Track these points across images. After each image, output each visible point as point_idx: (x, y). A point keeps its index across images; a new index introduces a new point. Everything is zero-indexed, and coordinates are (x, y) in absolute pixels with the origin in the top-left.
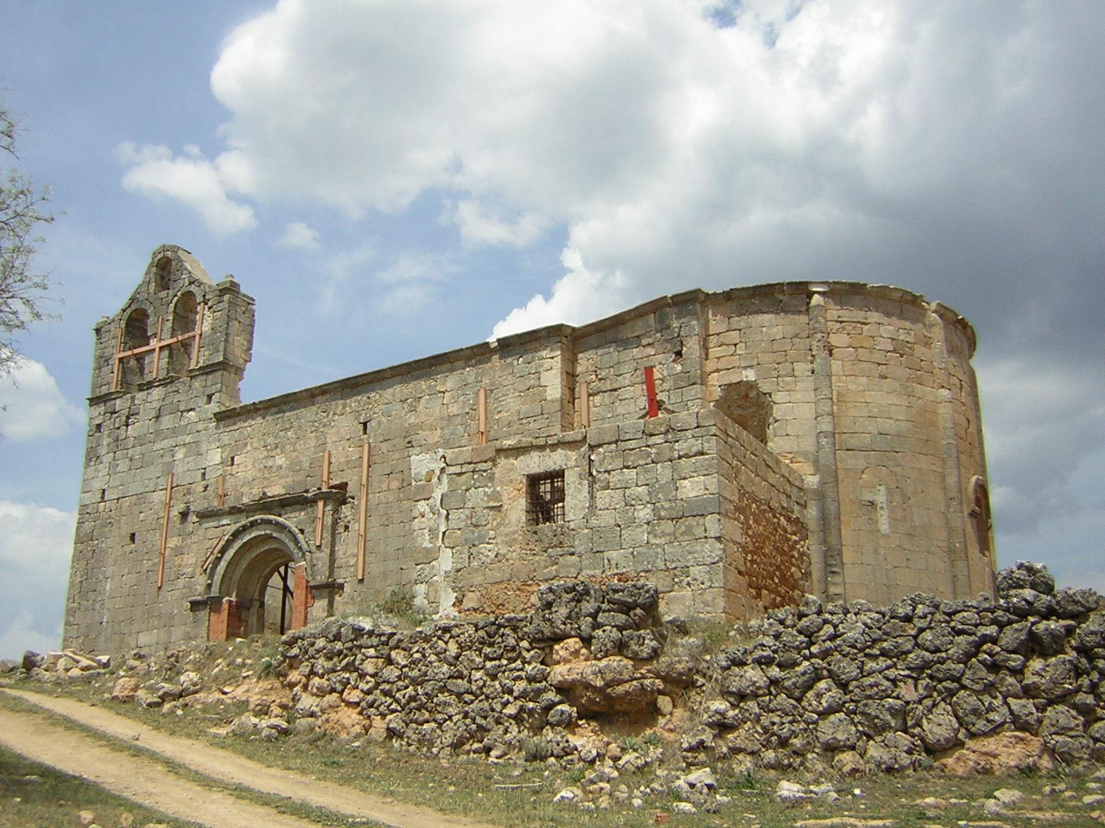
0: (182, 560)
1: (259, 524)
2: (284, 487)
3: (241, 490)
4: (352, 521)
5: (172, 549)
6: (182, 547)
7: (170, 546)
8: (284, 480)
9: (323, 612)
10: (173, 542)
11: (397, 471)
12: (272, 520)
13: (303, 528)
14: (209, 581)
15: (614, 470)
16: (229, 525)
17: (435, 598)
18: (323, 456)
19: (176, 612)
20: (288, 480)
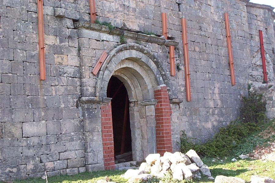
0: (62, 59)
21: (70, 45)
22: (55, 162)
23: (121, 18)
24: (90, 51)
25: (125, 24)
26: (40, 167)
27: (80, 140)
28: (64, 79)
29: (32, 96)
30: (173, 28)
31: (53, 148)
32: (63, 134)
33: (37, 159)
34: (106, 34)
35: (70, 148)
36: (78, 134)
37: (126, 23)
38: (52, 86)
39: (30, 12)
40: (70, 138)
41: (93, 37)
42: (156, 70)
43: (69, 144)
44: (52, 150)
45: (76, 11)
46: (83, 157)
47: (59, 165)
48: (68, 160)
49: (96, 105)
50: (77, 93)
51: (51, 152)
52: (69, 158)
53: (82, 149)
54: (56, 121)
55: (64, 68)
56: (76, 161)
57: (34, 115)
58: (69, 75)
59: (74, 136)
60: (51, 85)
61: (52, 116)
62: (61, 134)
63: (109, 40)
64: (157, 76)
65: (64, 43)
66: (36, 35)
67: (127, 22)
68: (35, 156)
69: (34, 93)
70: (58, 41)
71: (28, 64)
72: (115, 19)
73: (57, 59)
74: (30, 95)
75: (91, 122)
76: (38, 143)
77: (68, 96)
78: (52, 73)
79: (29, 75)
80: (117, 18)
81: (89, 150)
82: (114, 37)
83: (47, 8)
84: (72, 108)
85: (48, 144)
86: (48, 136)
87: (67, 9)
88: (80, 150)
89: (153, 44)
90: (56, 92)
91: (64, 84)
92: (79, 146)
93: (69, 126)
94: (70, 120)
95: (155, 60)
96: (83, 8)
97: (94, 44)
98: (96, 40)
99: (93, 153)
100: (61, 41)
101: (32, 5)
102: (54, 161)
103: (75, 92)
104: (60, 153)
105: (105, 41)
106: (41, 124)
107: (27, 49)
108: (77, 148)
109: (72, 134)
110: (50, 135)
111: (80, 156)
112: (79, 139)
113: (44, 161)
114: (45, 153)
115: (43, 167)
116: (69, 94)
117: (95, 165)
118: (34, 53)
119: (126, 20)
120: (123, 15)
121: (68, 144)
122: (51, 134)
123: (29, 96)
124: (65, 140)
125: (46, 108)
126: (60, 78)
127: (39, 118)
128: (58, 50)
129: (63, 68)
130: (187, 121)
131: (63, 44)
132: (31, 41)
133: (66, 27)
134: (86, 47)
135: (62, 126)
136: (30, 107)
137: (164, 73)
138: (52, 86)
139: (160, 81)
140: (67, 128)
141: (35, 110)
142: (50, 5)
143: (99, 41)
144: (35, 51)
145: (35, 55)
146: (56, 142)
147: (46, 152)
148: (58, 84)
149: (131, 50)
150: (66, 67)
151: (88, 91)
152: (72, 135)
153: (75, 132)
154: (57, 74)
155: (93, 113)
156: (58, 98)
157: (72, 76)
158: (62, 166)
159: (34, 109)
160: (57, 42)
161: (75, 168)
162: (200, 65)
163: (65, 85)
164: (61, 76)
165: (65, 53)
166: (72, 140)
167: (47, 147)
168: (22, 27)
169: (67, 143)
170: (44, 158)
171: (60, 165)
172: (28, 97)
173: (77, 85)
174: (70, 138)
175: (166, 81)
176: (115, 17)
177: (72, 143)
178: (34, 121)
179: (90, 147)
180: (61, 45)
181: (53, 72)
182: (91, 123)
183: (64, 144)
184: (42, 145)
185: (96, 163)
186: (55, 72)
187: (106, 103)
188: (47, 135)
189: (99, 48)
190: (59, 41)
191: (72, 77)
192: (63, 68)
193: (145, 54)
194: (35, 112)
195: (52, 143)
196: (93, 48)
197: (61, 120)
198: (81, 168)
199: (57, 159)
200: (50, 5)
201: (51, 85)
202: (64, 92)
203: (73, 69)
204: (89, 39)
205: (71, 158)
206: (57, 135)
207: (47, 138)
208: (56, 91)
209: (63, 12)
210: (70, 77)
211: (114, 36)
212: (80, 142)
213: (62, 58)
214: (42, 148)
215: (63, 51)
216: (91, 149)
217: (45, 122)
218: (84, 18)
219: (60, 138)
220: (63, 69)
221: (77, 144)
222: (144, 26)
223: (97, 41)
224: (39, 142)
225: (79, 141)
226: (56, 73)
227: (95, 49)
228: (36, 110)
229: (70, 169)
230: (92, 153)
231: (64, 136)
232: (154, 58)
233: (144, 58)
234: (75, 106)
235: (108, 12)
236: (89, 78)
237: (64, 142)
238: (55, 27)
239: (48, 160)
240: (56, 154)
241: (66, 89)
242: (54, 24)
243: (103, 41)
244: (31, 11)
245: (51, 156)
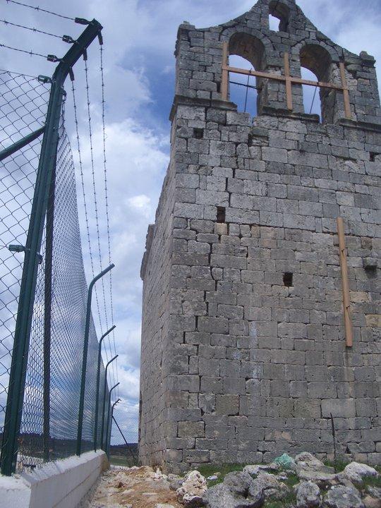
18: (341, 271)
33: (342, 447)
70: (370, 297)
100: (374, 298)
118: (336, 314)
170: (352, 446)
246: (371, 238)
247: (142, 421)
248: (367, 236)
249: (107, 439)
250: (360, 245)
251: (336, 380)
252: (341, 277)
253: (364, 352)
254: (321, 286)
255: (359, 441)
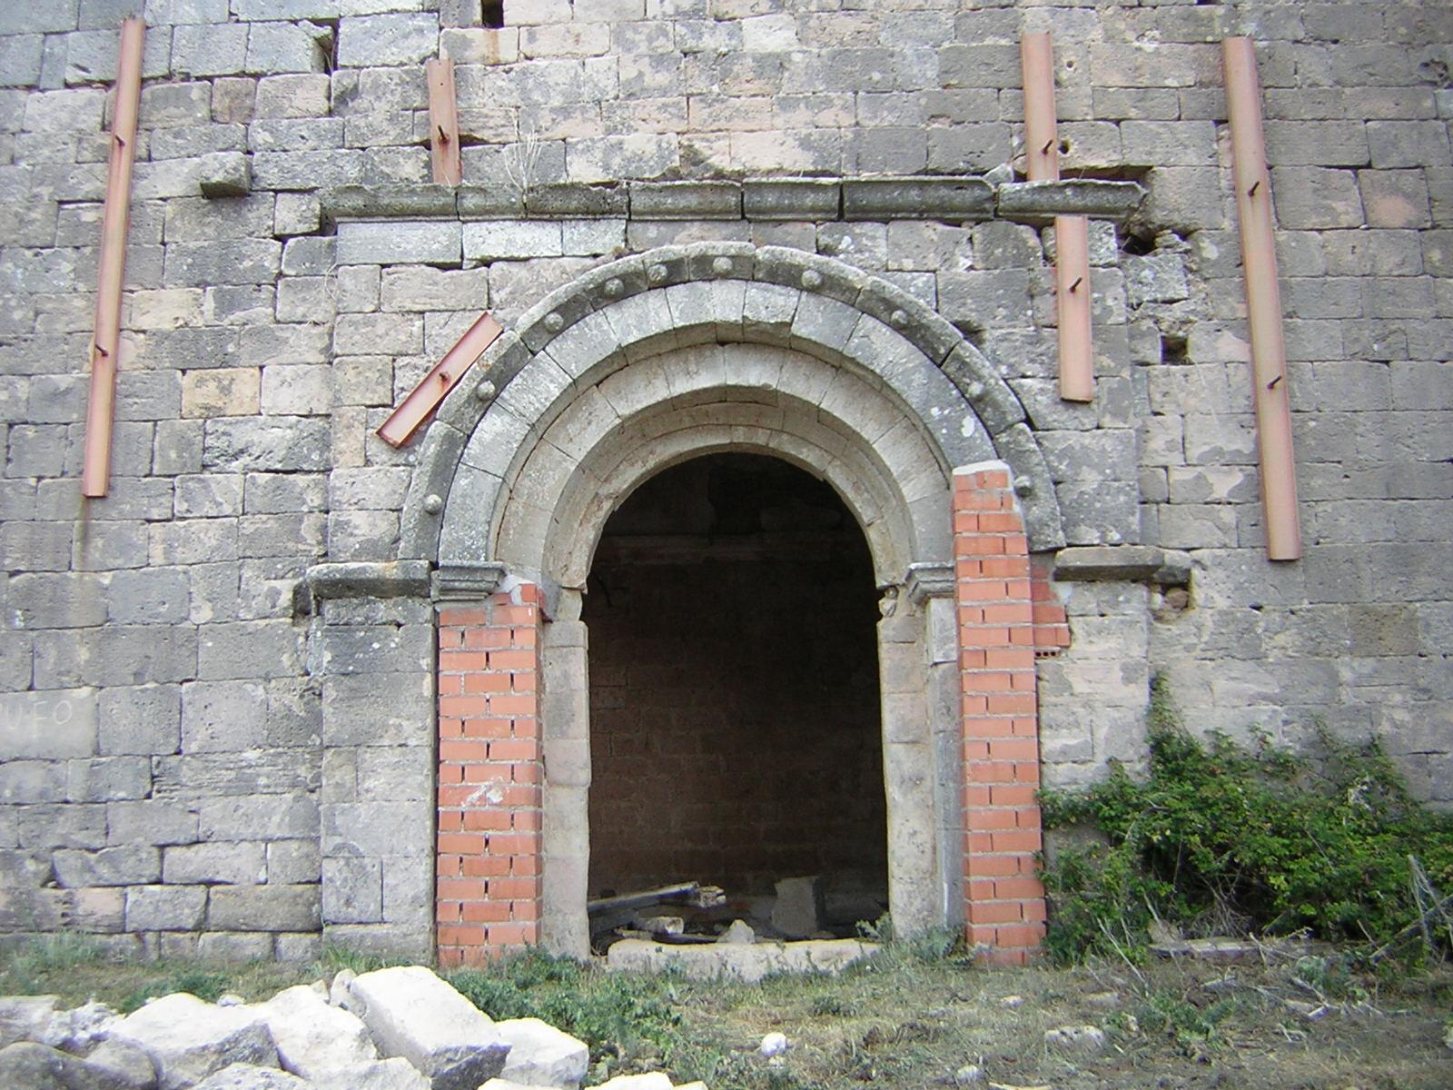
0: (225, 390)
1: (725, 276)
2: (805, 144)
3: (559, 132)
4: (1201, 324)
5: (160, 337)
6: (220, 336)
7: (146, 322)
8: (801, 115)
9: (1128, 680)
10: (167, 308)
11: (1395, 160)
12: (800, 269)
13: (973, 317)
14: (433, 499)
15: (1360, 189)
16: (564, 252)
17: (724, 154)
18: (99, 226)
19: (203, 614)
20: (826, 118)
21: (278, 317)
22: (129, 889)
23: (660, 127)
24: (381, 329)
25: (696, 153)
26: (44, 904)
27: (297, 791)
28: (227, 485)
29: (33, 572)
30: (1133, 113)
31: (122, 821)
32: (192, 755)
33: (31, 866)
34: (508, 223)
35: (225, 827)
36: (286, 759)
37: (697, 145)
38: (149, 521)
39: (73, 206)
40: (232, 774)
41: (406, 253)
42: (919, 378)
43: (225, 807)
44: (119, 831)
45: (343, 147)
46: (309, 882)
47: (150, 909)
48: (213, 889)
49: (396, 605)
50: (301, 547)
51: (111, 840)
52: (218, 878)
53: (303, 839)
54: (155, 690)
55: (233, 432)
56: (259, 898)
57: (36, 661)
58: (262, 463)
59: (263, 765)
60: (144, 516)
61: (134, 667)
62: (178, 753)
63: (524, 255)
64: (935, 411)
65: (242, 314)
66: (89, 300)
67: (712, 136)
68: (18, 852)
69: (45, 561)
70: (209, 304)
71: (30, 432)
72: (613, 138)
73: (196, 391)
74: (22, 568)
75: (355, 695)
76: (42, 794)
77: (240, 567)
78: (157, 459)
79: (33, 481)
80: (630, 129)
81: (327, 844)
82: (567, 235)
83: (168, 170)
84: (263, 623)
85: (92, 800)
86: (104, 759)
87: (285, 151)
88: (294, 845)
89: (894, 228)
90: (169, 550)
91: (225, 505)
92: (287, 819)
93: (226, 714)
94: (239, 688)
95: (897, 315)
96: (385, 123)
97: (413, 287)
98: (429, 265)
99: (347, 864)
100: (226, 304)
101: (90, 171)
102: (125, 886)
103: (290, 545)
104: (168, 849)
105: (500, 264)
106: (67, 702)
107: (36, 365)
108: (273, 831)
109: (252, 755)
110: (109, 759)
111: (289, 871)
112: (294, 786)
113: (66, 878)
114: (76, 842)
115: (60, 909)
116: (249, 553)
117: (361, 929)
118: (63, 381)
119: (698, 131)
120: (676, 104)
121: (214, 811)
122: (119, 751)
123: (22, 576)
124: (200, 787)
125: (104, 627)
126: (203, 481)
127: (60, 674)
128: (198, 351)
129: (224, 434)
130: (1266, 698)
131: (239, 316)
132: (61, 328)
133: (268, 233)
134: (357, 309)
135: (189, 712)
136: (19, 623)
137: (976, 389)
138: (149, 521)
139: (964, 439)
140: (218, 727)
141: (42, 639)
142: (183, 153)
143: (459, 267)
144: (74, 368)
145: (68, 391)
146: (142, 793)
147: (82, 838)
148: (188, 511)
149: (700, 284)
150: (242, 427)
151: (351, 535)
152: (244, 764)
153: (272, 746)
154: (185, 465)
155: (376, 646)
156: (181, 577)
157: (279, 466)
158: (167, 918)
159: (34, 634)
160: (202, 313)
161: (251, 935)
162: (1428, 311)
163: (227, 510)
164: (214, 469)
165: (244, 360)
166: (244, 786)
167: (91, 811)
168: (19, 276)
169: (211, 801)
170: (67, 863)
171: (157, 909)
172: (14, 581)
173: (305, 509)
174: (232, 774)
175: (1003, 438)
176: (609, 131)
177: (242, 801)
178: (30, 688)
179: (333, 830)
180: (226, 322)
181: (164, 457)
182: (349, 699)
183: (193, 805)
184: (67, 802)
185: (364, 919)
186: (173, 455)
187: (461, 590)
188: (97, 752)
189: (451, 304)
190: (213, 305)
191: (277, 471)
192: (229, 429)
193: (813, 290)
194: (39, 647)
195: (122, 794)
196: (408, 305)
197: (186, 685)
198: (291, 936)
199: (141, 876)
200: (183, 153)
201: (148, 516)
202: (218, 548)
203: (288, 431)
204: (383, 266)
205: (229, 880)
206: (155, 759)
207: (93, 772)
208: (171, 546)
209: (228, 165)
210: (268, 471)
211: (566, 227)
212: (296, 799)
213: (226, 383)
214: (61, 819)
215: (231, 348)
216: (338, 840)
217: (93, 694)
218: (387, 170)
219: (173, 772)
220: (225, 438)
221: (276, 812)
222: (857, 135)
223: (444, 267)
224: (50, 785)
225: (289, 796)
226: (180, 456)
227: (422, 313)
228: (49, 636)
229: (220, 934)
230: (342, 862)
231: (195, 763)
232: (891, 306)
233: (813, 320)
234: (284, 616)
235: (564, 112)
236: (361, 462)
237: (192, 794)
238: (199, 244)
239: (87, 876)
240: (137, 850)
241: (233, 533)
242: (199, 234)
243: (487, 263)
244: (79, 197)
245: (111, 860)
246: (257, 76)
247: (672, 429)
248: (243, 74)
249: (788, 221)
250: (202, 113)
251: (32, 624)
252: (98, 251)
253: (155, 514)
254: (20, 285)
255: (97, 843)
